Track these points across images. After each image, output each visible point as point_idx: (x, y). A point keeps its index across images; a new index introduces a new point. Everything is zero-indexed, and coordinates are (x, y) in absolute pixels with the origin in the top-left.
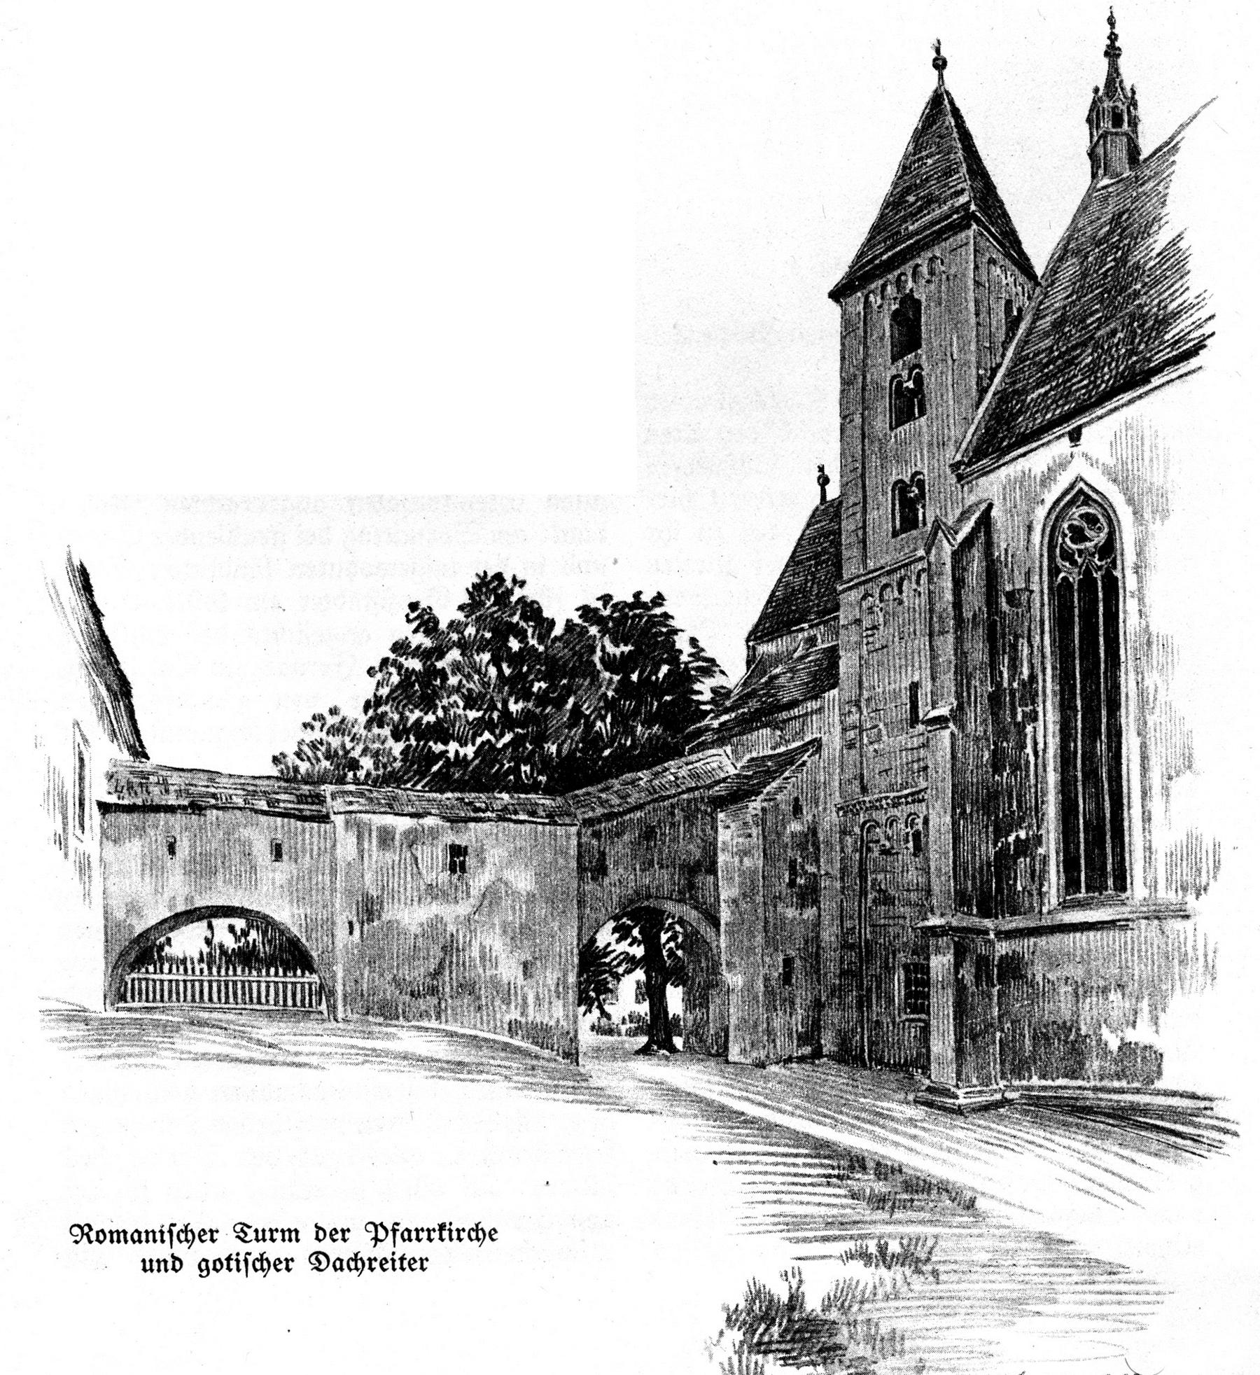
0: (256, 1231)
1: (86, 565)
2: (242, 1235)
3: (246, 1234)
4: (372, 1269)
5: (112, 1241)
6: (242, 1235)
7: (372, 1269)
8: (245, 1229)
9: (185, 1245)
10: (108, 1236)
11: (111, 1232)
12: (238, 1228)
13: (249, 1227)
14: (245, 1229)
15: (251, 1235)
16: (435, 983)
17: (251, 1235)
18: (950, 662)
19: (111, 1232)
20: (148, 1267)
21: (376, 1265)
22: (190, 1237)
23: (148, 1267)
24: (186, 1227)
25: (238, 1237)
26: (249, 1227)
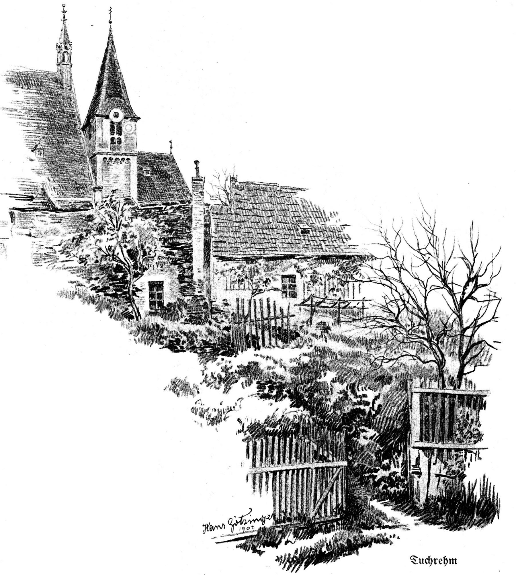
0: (420, 559)
1: (487, 403)
2: (414, 561)
3: (415, 560)
4: (435, 563)
5: (450, 563)
6: (414, 561)
7: (435, 563)
8: (415, 558)
9: (428, 565)
10: (449, 561)
11: (450, 560)
12: (412, 558)
13: (417, 557)
14: (415, 558)
15: (418, 561)
16: (179, 225)
17: (418, 561)
18: (169, 257)
19: (450, 560)
20: (454, 561)
21: (437, 561)
22: (430, 561)
23: (454, 561)
24: (429, 557)
25: (412, 562)
26: (417, 557)
